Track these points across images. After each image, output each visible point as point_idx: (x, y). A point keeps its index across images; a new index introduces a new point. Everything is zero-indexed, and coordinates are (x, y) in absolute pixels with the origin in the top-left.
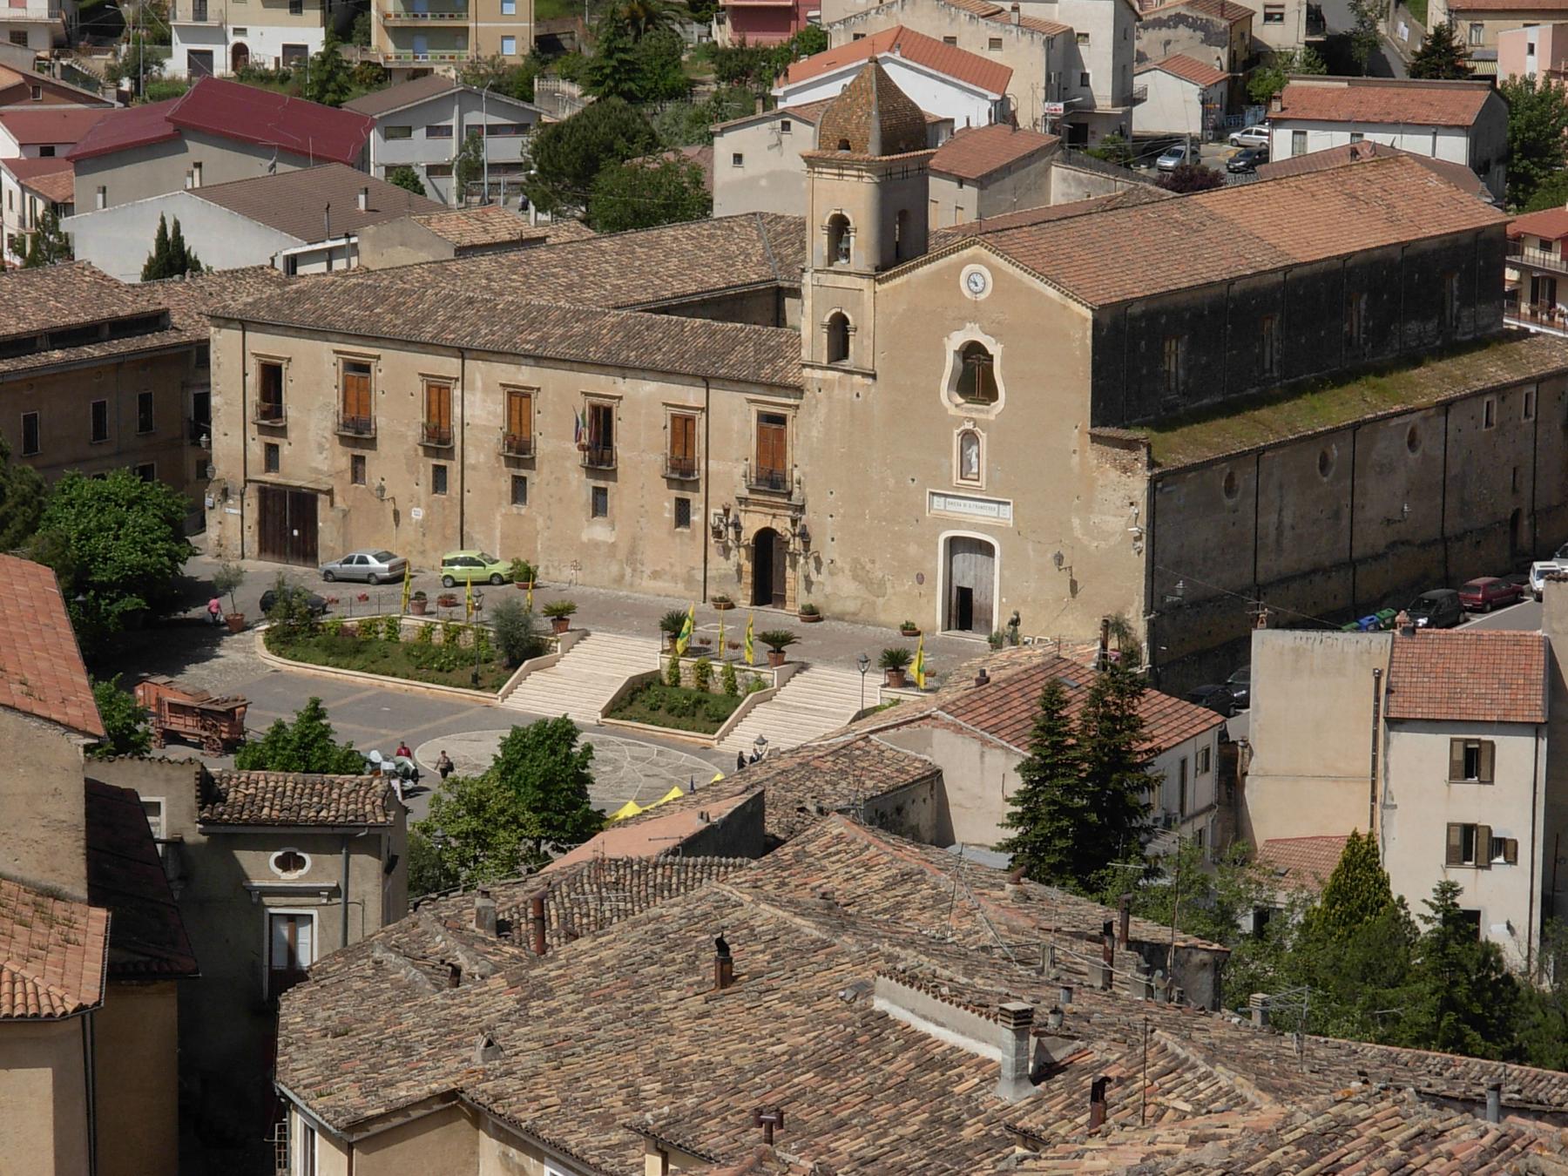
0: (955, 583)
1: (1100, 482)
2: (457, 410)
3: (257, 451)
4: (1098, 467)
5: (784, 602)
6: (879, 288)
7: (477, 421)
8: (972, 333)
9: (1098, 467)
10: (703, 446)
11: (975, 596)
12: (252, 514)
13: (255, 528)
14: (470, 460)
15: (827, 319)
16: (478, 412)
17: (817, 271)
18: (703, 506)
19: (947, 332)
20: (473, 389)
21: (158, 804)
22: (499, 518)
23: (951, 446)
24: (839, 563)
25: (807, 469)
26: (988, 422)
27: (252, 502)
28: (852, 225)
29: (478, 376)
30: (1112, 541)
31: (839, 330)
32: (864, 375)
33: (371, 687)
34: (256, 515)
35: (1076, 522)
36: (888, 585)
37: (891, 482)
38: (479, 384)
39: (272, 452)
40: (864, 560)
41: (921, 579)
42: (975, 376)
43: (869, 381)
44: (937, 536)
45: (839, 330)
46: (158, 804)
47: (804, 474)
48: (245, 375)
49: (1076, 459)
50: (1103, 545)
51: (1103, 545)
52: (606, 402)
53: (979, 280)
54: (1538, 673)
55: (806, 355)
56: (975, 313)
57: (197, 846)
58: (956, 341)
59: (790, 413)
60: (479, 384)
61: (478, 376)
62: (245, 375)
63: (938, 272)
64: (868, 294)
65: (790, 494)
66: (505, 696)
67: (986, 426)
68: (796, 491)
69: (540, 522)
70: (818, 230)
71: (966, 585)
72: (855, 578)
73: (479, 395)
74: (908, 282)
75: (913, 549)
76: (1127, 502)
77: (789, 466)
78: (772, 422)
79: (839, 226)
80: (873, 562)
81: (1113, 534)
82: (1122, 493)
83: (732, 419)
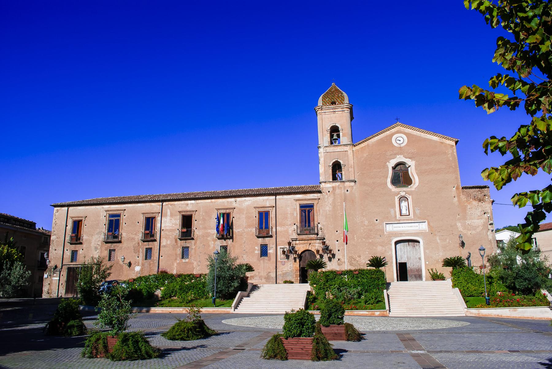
0: (398, 261)
1: (469, 207)
2: (158, 225)
3: (68, 254)
4: (467, 201)
6: (354, 149)
7: (167, 228)
8: (400, 158)
10: (274, 222)
11: (408, 265)
12: (64, 279)
13: (64, 284)
14: (164, 243)
15: (331, 164)
16: (167, 224)
18: (274, 246)
19: (388, 160)
20: (166, 216)
22: (175, 265)
23: (395, 204)
25: (324, 223)
26: (411, 191)
27: (64, 273)
28: (340, 128)
29: (169, 211)
30: (478, 230)
31: (337, 167)
32: (352, 181)
34: (65, 279)
35: (459, 224)
37: (366, 223)
38: (169, 213)
39: (74, 254)
40: (356, 256)
42: (401, 177)
43: (353, 184)
44: (391, 241)
45: (337, 167)
47: (323, 225)
48: (66, 226)
50: (474, 232)
51: (474, 232)
52: (228, 211)
54: (347, 349)
55: (322, 179)
56: (401, 151)
57: (459, 89)
58: (393, 162)
59: (315, 202)
60: (169, 213)
61: (169, 211)
62: (66, 226)
63: (381, 139)
64: (350, 153)
65: (317, 234)
66: (236, 307)
67: (409, 193)
68: (320, 233)
69: (195, 263)
71: (403, 261)
73: (168, 218)
74: (368, 145)
77: (316, 223)
78: (307, 212)
79: (334, 130)
80: (360, 256)
81: (478, 226)
82: (480, 210)
83: (287, 208)
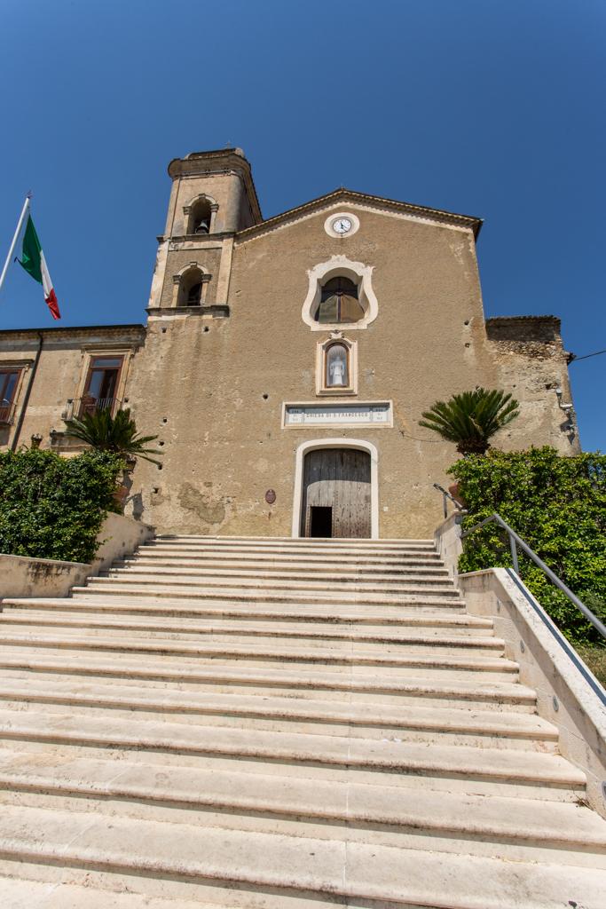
0: (310, 503)
4: (499, 355)
5: (495, 399)
8: (339, 262)
9: (499, 355)
17: (175, 239)
21: (389, 404)
24: (164, 492)
25: (138, 402)
33: (108, 734)
36: (228, 508)
41: (271, 497)
46: (389, 404)
49: (471, 351)
53: (346, 224)
70: (180, 211)
71: (323, 503)
72: (185, 504)
75: (262, 466)
76: (543, 384)
82: (535, 376)
